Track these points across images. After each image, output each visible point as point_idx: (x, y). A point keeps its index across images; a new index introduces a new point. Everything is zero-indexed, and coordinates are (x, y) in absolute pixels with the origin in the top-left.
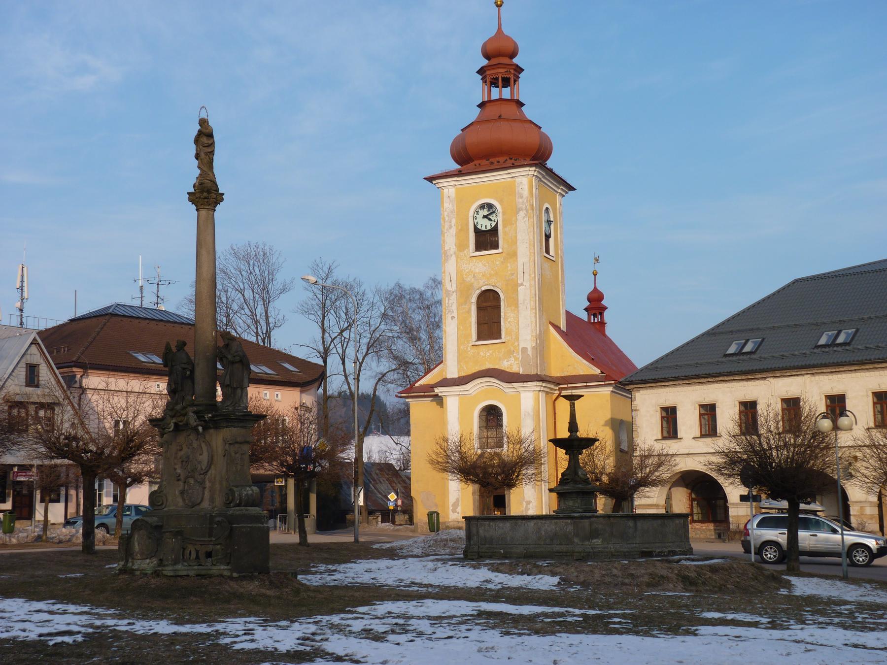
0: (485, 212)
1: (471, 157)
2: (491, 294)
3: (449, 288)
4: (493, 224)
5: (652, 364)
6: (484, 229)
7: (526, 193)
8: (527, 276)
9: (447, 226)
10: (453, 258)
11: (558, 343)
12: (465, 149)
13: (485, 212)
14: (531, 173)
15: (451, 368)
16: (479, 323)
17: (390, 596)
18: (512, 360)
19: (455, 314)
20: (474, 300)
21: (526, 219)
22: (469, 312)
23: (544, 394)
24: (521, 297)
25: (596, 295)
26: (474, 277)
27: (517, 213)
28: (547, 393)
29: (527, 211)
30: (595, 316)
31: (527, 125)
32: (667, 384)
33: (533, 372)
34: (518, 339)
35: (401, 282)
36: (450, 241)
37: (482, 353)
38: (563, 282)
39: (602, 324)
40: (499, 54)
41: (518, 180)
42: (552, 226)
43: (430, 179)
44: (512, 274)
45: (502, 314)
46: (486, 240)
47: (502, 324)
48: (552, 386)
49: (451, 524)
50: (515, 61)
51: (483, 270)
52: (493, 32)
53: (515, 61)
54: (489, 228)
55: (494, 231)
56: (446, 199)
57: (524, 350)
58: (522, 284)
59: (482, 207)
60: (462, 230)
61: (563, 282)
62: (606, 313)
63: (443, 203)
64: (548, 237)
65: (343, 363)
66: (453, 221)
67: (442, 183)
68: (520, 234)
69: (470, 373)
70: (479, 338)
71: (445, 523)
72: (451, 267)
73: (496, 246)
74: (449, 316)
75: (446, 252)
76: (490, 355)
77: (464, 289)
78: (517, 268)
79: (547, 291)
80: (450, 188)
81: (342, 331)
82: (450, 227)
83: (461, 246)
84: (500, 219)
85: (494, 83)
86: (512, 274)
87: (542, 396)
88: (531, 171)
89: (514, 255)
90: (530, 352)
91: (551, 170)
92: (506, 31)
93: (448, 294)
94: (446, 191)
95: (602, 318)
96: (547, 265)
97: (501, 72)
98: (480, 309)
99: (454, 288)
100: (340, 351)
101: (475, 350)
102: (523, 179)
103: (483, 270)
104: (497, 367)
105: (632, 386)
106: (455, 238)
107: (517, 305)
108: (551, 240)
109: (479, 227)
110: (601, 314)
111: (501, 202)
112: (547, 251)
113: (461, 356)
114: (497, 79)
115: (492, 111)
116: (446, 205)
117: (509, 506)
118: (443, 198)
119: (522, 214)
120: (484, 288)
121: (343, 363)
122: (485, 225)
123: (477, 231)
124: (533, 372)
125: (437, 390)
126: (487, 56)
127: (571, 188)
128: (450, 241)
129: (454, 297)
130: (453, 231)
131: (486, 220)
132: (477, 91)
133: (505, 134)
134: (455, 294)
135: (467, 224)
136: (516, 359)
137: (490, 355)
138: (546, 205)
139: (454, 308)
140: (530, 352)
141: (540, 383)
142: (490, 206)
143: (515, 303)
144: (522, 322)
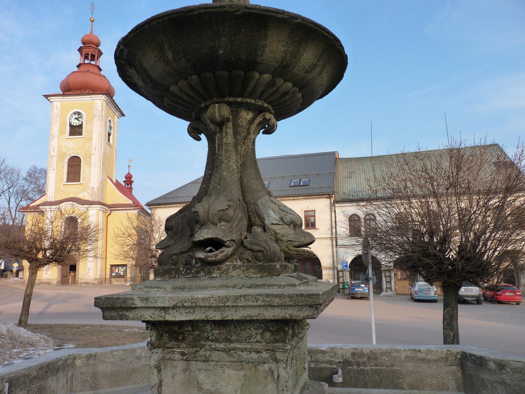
0: (76, 116)
1: (69, 89)
2: (76, 158)
3: (53, 154)
4: (80, 123)
5: (163, 196)
6: (75, 125)
7: (99, 108)
8: (97, 150)
9: (54, 121)
10: (56, 138)
11: (111, 188)
12: (68, 85)
13: (76, 116)
14: (104, 98)
15: (51, 195)
16: (69, 173)
17: (212, 169)
18: (85, 193)
19: (55, 168)
20: (66, 161)
21: (99, 121)
22: (63, 167)
23: (102, 212)
24: (93, 161)
25: (129, 176)
26: (67, 149)
27: (94, 118)
28: (104, 212)
29: (99, 117)
30: (128, 184)
31: (102, 78)
32: (172, 206)
33: (97, 200)
34: (89, 182)
35: (36, 165)
36: (55, 129)
37: (68, 189)
38: (116, 159)
39: (131, 188)
40: (90, 43)
41: (96, 101)
42: (112, 130)
43: (46, 96)
44: (89, 149)
45: (82, 169)
46: (76, 130)
47: (81, 174)
48: (107, 208)
49: (44, 281)
50: (99, 48)
51: (73, 146)
52: (89, 32)
53: (99, 48)
54: (78, 124)
55: (81, 126)
56: (55, 108)
57: (93, 188)
58: (94, 154)
59: (75, 113)
60: (62, 125)
61: (116, 159)
62: (133, 184)
63: (53, 109)
64: (109, 135)
65: (9, 204)
66: (58, 119)
67: (52, 99)
68: (95, 129)
69: (60, 199)
70: (68, 181)
71: (40, 280)
72: (54, 143)
73: (81, 135)
74: (51, 169)
75: (52, 135)
76: (73, 190)
77: (61, 155)
78: (91, 147)
79: (107, 163)
80: (58, 102)
81: (9, 188)
82: (56, 122)
83: (61, 133)
84: (84, 120)
85: (86, 57)
86: (89, 149)
87: (101, 213)
88: (103, 97)
89: (90, 139)
90: (96, 190)
91: (114, 101)
92: (95, 33)
93: (52, 157)
94: (55, 104)
95: (131, 186)
96: (108, 147)
97: (90, 51)
98: (69, 166)
99: (56, 154)
100: (8, 198)
101: (65, 187)
102: (99, 101)
103: (73, 146)
104: (76, 196)
105: (152, 207)
106: (58, 129)
107: (90, 165)
108: (111, 137)
109: (72, 123)
110: (131, 184)
111: (85, 111)
112: (109, 141)
113: (57, 189)
114: (88, 54)
115: (83, 68)
116: (55, 111)
117: (78, 271)
118: (53, 107)
119: (96, 118)
120: (72, 155)
121: (9, 204)
122: (76, 123)
123: (71, 126)
124: (97, 200)
125: (40, 207)
126: (84, 43)
127: (123, 115)
128: (55, 129)
129: (55, 159)
130: (58, 124)
131: (76, 120)
132: (77, 58)
133: (91, 79)
134: (55, 157)
135: (66, 122)
136: (88, 193)
137: (73, 190)
138: (109, 118)
139: (55, 164)
140: (96, 190)
141: (100, 206)
142: (79, 113)
143: (89, 164)
144: (92, 173)
